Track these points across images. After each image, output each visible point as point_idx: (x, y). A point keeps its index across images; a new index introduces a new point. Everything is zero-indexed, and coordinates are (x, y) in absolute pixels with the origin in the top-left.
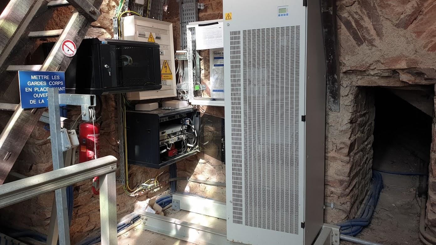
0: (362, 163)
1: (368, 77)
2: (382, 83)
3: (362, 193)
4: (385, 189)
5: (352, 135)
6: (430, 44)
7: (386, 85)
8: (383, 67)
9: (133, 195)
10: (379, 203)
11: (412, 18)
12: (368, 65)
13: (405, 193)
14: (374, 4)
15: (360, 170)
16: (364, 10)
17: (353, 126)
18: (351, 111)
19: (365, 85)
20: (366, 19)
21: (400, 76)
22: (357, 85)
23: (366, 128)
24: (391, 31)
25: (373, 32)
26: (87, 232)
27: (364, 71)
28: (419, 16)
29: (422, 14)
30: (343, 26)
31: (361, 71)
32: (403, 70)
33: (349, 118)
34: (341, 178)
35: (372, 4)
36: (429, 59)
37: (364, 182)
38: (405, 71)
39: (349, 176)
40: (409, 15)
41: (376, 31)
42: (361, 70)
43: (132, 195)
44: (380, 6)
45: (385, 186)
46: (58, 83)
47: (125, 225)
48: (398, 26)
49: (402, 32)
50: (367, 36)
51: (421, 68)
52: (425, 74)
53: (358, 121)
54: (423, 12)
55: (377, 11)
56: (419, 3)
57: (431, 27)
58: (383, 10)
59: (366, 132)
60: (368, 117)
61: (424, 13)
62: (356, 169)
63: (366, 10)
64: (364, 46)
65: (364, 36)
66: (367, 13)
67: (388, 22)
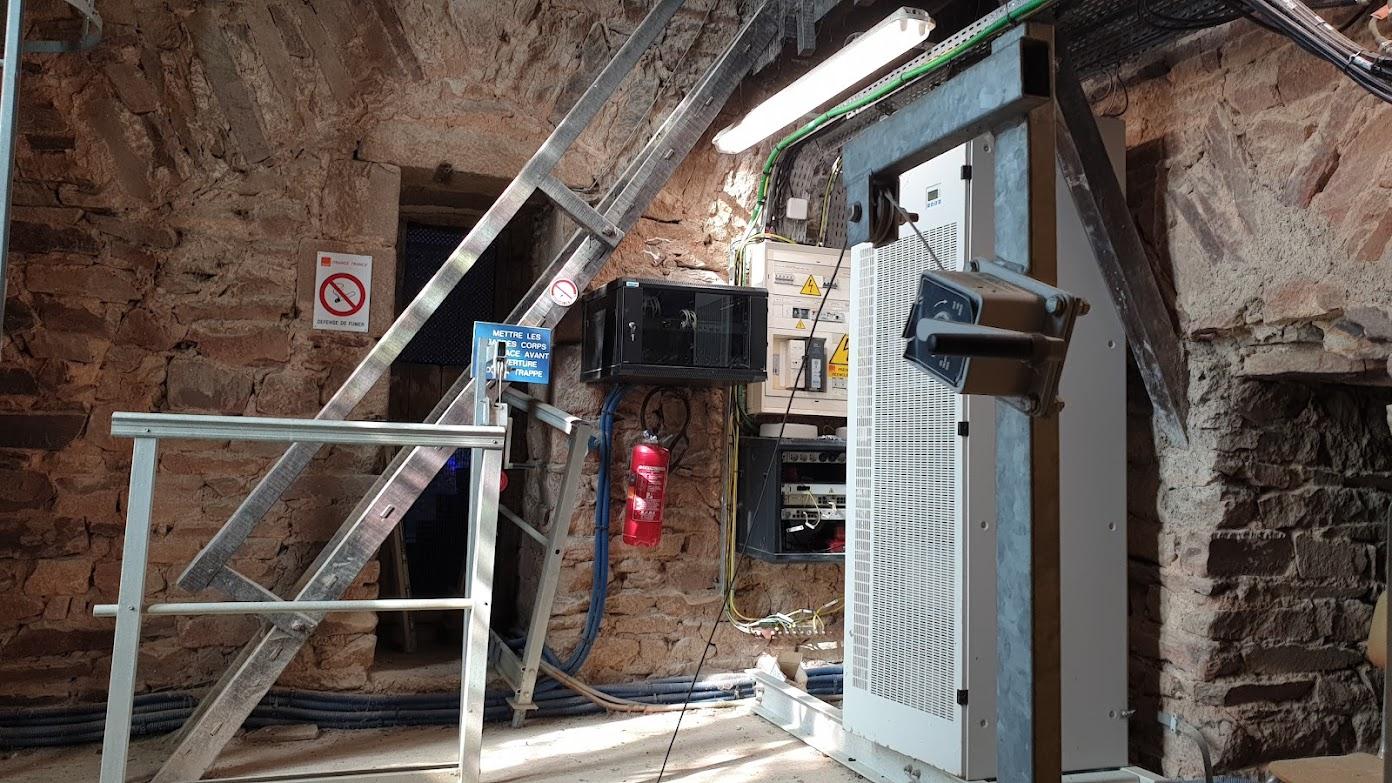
9: (747, 631)
20: (1223, 192)
25: (1236, 223)
26: (631, 675)
30: (1181, 218)
34: (1192, 639)
40: (1307, 169)
43: (745, 628)
46: (537, 346)
47: (717, 693)
56: (1325, 135)
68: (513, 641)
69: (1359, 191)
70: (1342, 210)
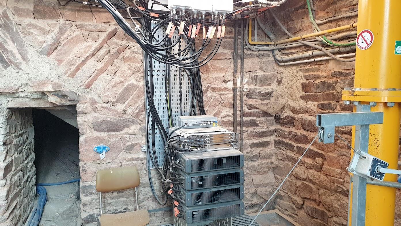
0: (23, 182)
1: (18, 99)
2: (34, 104)
3: (25, 211)
4: (49, 201)
5: (8, 157)
6: (69, 71)
7: (37, 106)
8: (32, 90)
10: (43, 216)
11: (52, 48)
12: (17, 87)
13: (66, 200)
14: (17, 30)
15: (21, 190)
16: (7, 34)
17: (7, 148)
18: (3, 134)
19: (16, 107)
20: (10, 42)
21: (48, 98)
22: (8, 107)
23: (24, 147)
24: (35, 57)
25: (18, 56)
27: (14, 93)
28: (58, 47)
29: (61, 46)
31: (10, 93)
32: (50, 92)
33: (2, 140)
35: (15, 29)
36: (70, 83)
37: (27, 200)
38: (52, 93)
39: (7, 200)
40: (50, 45)
41: (21, 55)
42: (9, 92)
44: (22, 32)
45: (49, 198)
48: (41, 53)
49: (45, 58)
50: (13, 60)
51: (64, 91)
52: (68, 96)
53: (14, 142)
54: (61, 44)
55: (20, 37)
56: (57, 36)
57: (69, 57)
58: (27, 37)
59: (25, 151)
60: (25, 137)
61: (62, 44)
62: (15, 191)
63: (9, 35)
64: (11, 69)
65: (10, 59)
66: (10, 37)
67: (32, 48)
68: (349, 144)
69: (68, 56)
70: (62, 60)
